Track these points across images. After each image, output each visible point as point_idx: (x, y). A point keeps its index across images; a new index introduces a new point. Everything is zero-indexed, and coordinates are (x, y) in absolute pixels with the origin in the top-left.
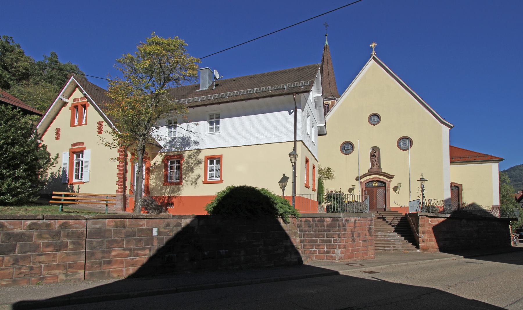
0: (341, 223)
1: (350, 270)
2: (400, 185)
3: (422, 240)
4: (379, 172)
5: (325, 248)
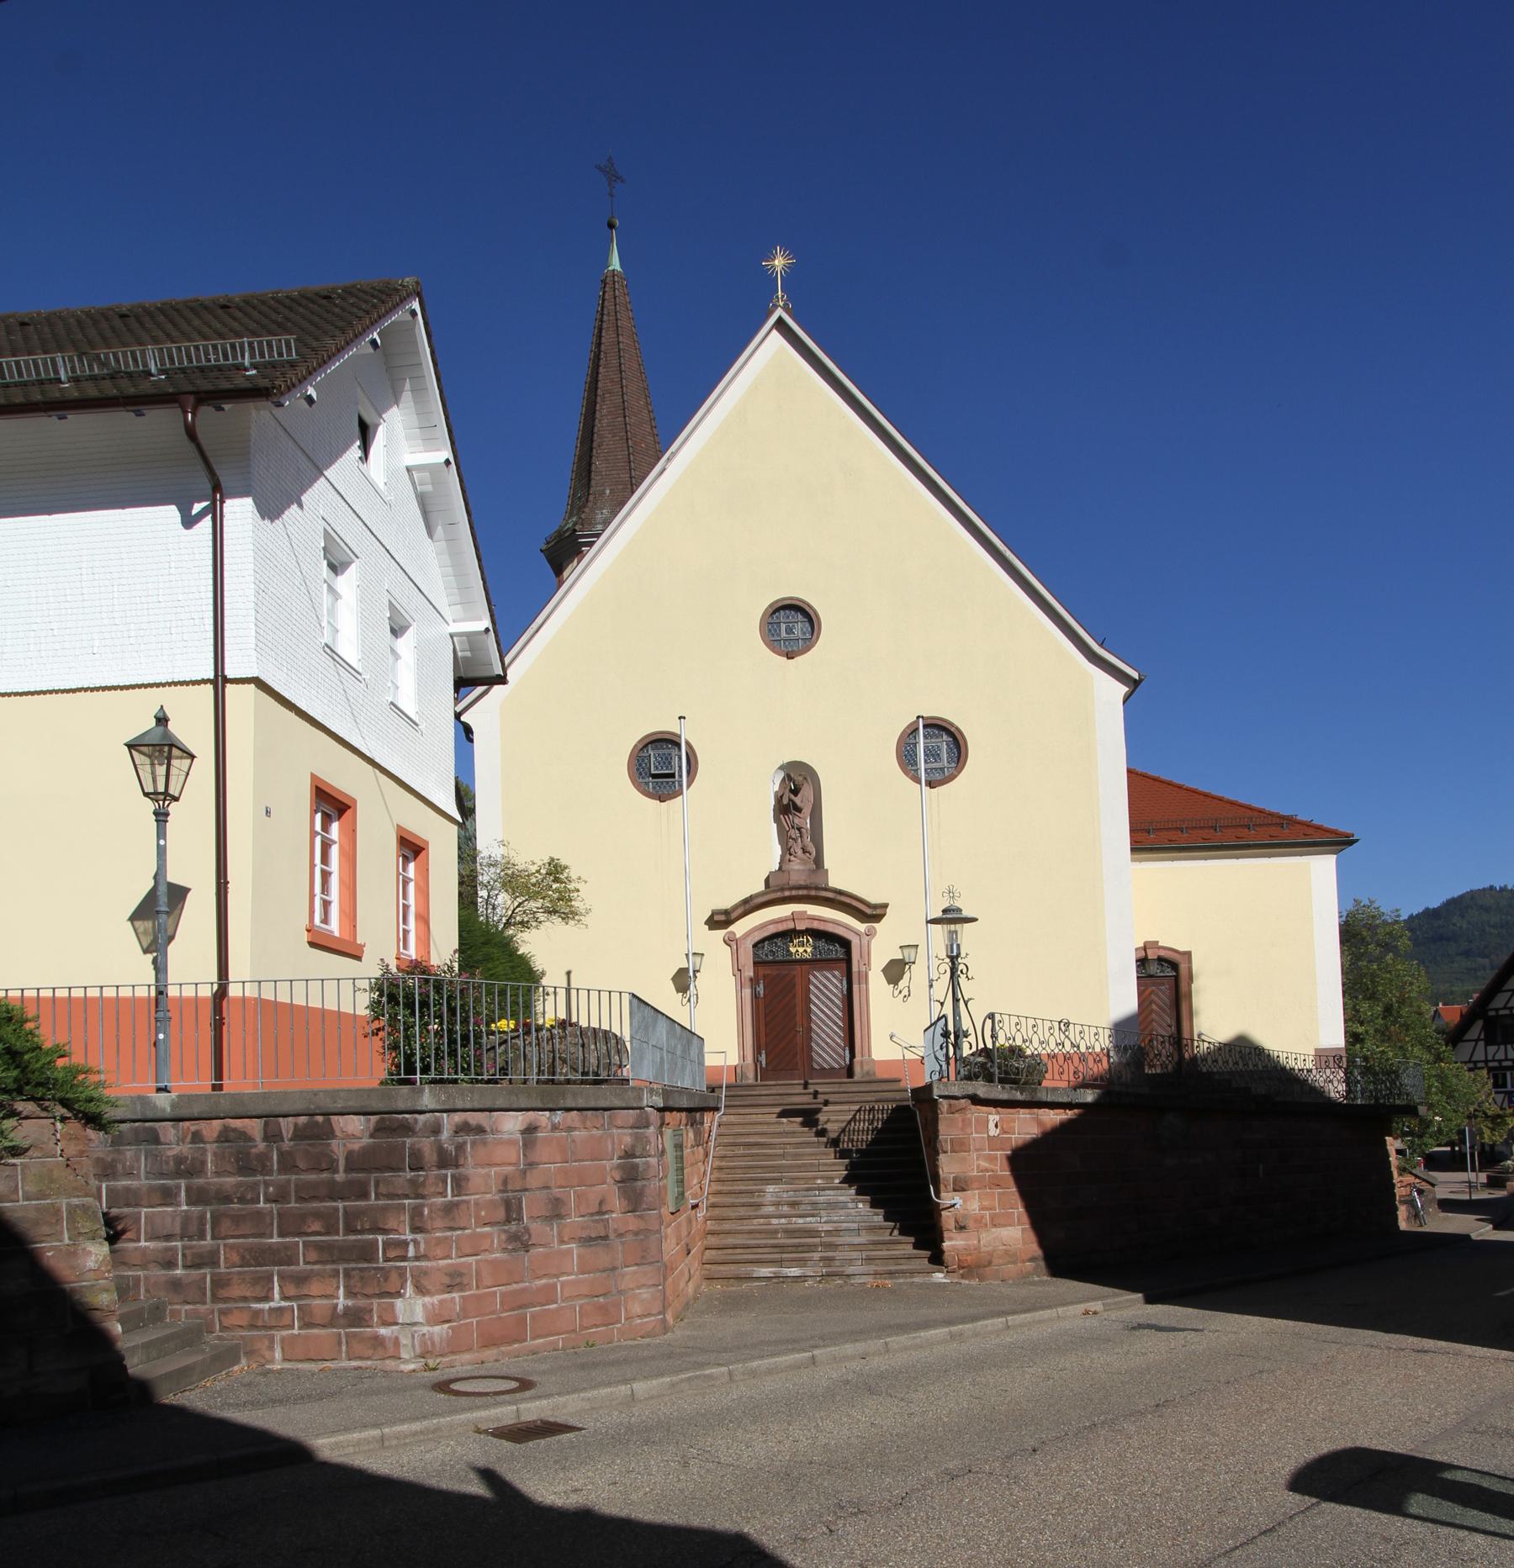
0: (426, 1145)
1: (398, 1428)
2: (913, 951)
3: (956, 1222)
4: (817, 888)
5: (341, 1291)
